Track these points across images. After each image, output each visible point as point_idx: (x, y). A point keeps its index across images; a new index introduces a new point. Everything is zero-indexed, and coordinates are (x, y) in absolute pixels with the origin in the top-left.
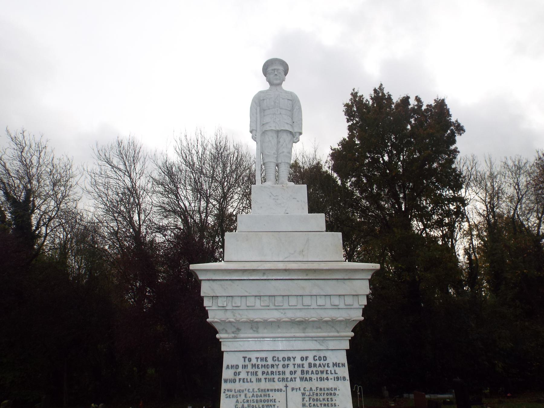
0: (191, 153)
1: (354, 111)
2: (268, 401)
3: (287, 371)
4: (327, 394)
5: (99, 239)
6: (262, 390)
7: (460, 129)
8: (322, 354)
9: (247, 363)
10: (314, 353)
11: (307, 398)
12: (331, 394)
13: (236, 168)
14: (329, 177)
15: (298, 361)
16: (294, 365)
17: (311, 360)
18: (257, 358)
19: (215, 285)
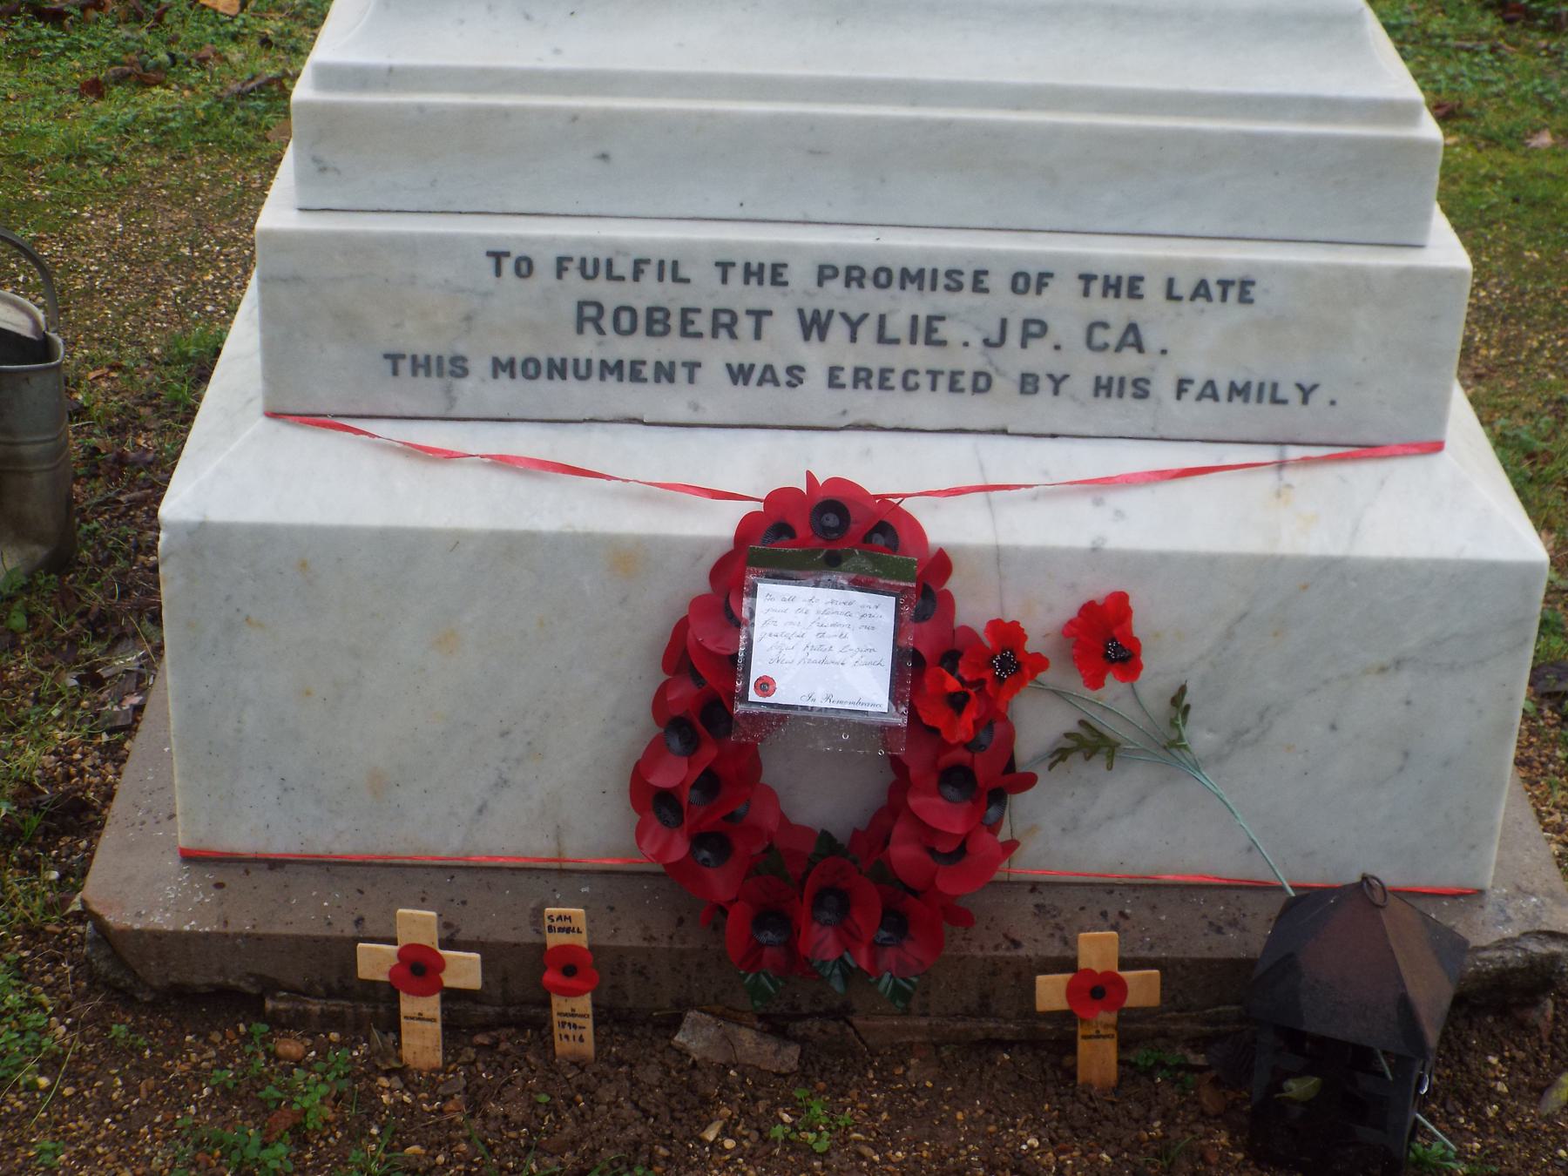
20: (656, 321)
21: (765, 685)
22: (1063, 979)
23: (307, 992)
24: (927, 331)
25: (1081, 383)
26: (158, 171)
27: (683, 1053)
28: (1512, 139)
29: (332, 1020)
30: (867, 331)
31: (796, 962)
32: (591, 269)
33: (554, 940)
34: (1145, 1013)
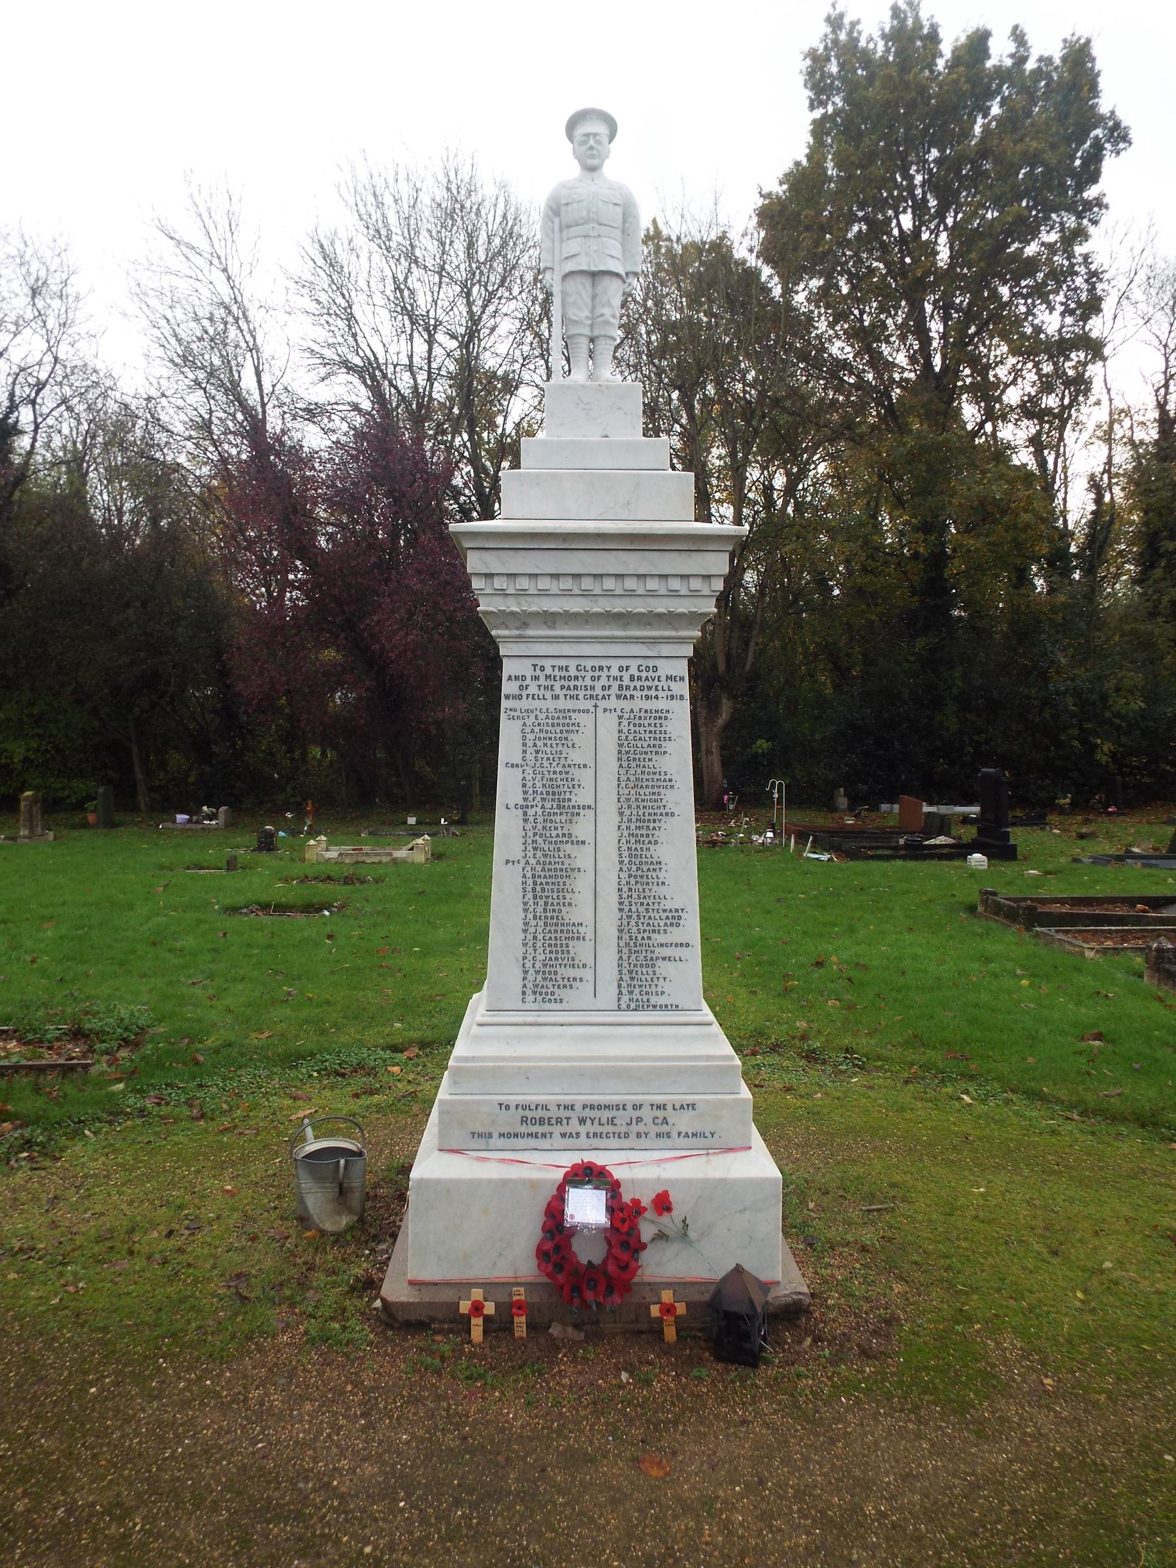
0: (380, 205)
1: (831, 75)
2: (568, 725)
3: (598, 685)
4: (655, 718)
5: (161, 437)
6: (560, 711)
7: (1119, 135)
8: (651, 663)
9: (538, 672)
10: (639, 661)
11: (625, 723)
12: (660, 718)
13: (504, 244)
14: (752, 275)
15: (615, 672)
16: (609, 677)
17: (634, 671)
18: (553, 667)
19: (489, 557)
20: (541, 1121)
21: (572, 1217)
22: (658, 1306)
23: (444, 1321)
24: (611, 1121)
25: (652, 1135)
26: (378, 1119)
27: (551, 1335)
28: (809, 1096)
29: (451, 1331)
30: (596, 1122)
31: (585, 1305)
32: (524, 1108)
33: (515, 1298)
34: (681, 1316)
